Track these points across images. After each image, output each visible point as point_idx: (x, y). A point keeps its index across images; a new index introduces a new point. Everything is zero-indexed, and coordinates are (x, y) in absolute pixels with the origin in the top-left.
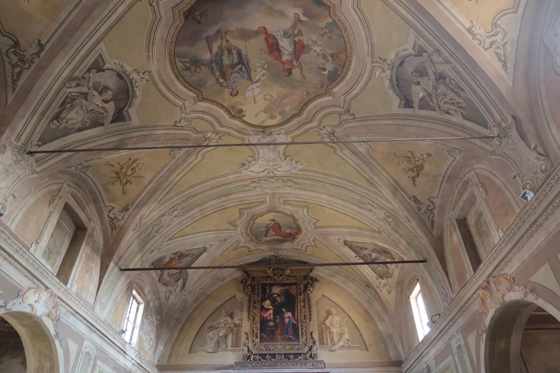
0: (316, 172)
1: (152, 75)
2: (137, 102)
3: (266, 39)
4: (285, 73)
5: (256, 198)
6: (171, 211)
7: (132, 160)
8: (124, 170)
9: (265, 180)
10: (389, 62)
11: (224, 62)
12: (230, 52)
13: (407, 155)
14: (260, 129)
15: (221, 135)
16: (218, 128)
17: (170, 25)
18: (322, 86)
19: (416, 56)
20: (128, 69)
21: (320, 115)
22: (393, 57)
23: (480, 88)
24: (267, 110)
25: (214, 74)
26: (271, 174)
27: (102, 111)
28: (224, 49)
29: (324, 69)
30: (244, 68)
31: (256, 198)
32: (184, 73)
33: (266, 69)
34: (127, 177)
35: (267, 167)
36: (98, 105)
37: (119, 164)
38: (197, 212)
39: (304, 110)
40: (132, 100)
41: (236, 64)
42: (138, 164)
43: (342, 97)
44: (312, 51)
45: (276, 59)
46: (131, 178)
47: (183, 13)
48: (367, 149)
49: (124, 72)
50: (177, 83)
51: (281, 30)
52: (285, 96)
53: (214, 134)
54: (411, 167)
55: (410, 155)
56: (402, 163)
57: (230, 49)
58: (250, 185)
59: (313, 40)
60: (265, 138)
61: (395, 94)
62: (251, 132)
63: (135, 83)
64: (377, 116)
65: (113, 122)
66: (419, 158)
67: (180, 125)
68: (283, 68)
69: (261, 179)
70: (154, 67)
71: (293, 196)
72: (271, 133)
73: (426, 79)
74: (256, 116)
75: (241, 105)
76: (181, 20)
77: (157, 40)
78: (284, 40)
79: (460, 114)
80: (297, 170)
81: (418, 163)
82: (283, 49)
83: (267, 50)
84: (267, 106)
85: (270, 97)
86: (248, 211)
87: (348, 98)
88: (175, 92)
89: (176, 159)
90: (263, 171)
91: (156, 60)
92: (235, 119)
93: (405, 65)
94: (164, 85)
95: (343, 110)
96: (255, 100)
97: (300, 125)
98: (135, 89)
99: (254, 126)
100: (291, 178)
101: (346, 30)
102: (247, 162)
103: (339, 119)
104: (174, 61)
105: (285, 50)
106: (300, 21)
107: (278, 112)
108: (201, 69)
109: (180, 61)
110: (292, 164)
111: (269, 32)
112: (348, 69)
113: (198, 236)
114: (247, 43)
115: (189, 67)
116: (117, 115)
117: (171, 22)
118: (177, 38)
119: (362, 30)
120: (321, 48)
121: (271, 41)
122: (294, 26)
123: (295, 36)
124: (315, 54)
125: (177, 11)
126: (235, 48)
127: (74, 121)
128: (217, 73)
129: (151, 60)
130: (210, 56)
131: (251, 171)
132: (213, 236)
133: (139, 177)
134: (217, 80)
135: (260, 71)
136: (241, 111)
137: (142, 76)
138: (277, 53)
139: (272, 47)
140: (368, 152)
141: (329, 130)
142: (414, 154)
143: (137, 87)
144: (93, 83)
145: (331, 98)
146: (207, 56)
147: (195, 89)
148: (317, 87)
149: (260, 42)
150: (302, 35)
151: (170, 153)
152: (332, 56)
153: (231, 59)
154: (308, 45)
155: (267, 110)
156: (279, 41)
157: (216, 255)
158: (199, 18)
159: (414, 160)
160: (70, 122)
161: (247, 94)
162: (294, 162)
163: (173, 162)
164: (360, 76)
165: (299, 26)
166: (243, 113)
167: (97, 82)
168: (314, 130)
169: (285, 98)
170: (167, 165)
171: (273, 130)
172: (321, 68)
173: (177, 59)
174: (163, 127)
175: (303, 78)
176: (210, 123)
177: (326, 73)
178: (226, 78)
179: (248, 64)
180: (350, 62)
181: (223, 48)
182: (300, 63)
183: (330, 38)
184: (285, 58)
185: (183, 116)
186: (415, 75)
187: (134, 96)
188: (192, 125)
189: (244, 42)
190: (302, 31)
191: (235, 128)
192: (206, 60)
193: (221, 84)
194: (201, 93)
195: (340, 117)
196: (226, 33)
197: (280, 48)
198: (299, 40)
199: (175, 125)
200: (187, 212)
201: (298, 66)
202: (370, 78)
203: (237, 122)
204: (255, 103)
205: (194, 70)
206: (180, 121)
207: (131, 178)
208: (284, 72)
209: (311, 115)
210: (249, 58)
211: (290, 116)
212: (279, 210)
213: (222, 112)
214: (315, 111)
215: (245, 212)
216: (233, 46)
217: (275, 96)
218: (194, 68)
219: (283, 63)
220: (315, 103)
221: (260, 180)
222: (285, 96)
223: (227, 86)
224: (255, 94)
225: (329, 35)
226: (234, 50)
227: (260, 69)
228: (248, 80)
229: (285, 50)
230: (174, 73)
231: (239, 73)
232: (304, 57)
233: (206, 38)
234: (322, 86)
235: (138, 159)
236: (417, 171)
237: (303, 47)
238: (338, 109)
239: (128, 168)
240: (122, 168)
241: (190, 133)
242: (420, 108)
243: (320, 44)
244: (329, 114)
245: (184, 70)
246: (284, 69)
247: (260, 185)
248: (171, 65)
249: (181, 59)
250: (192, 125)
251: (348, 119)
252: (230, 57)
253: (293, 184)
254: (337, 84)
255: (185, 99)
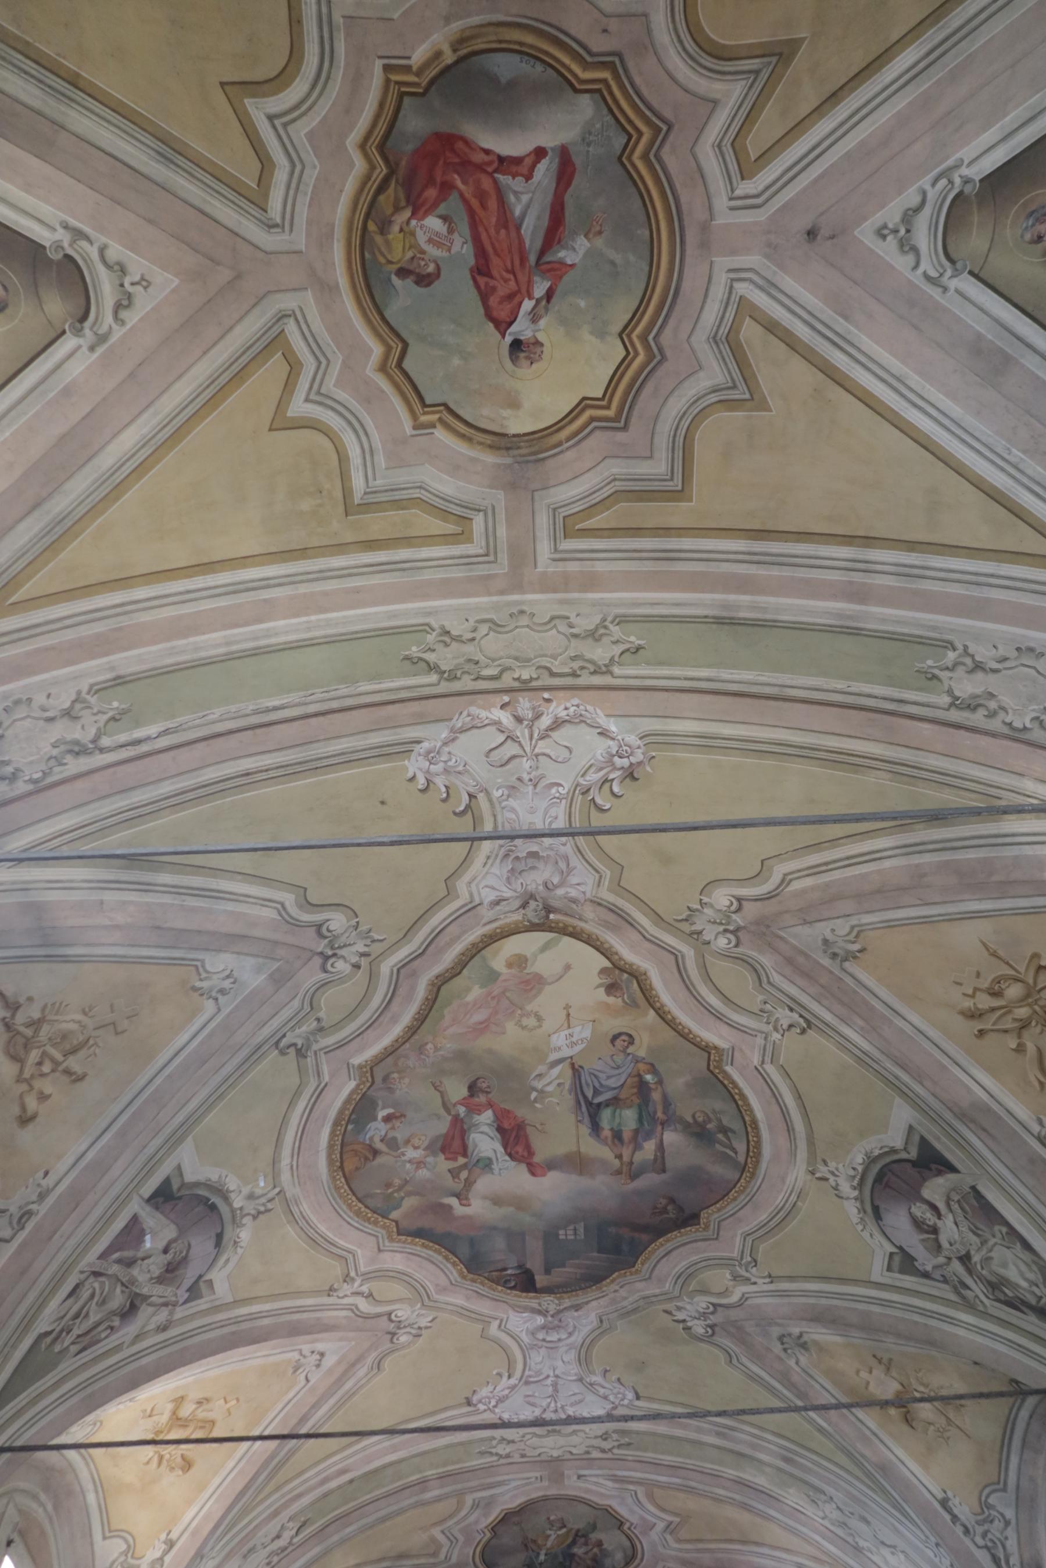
0: (348, 759)
1: (809, 1164)
2: (873, 1144)
3: (531, 1153)
4: (484, 1085)
5: (600, 567)
6: (977, 718)
7: (976, 1025)
8: (1022, 1012)
9: (553, 674)
10: (245, 1220)
11: (636, 1116)
12: (617, 1135)
13: (82, 1054)
14: (557, 922)
15: (686, 927)
16: (688, 952)
17: (731, 1219)
18: (385, 1079)
19: (200, 1276)
20: (852, 1209)
21: (377, 1000)
22: (241, 1235)
23: (56, 1400)
24: (534, 984)
25: (665, 1097)
26: (524, 705)
27: (955, 1207)
28: (630, 1142)
29: (387, 1119)
30: (589, 1094)
31: (600, 567)
32: (736, 1125)
33: (534, 1089)
34: (1031, 981)
35: (542, 747)
36: (956, 1224)
37: (1020, 1049)
38: (883, 602)
39: (427, 999)
40: (880, 1156)
41: (607, 1105)
42: (973, 996)
43: (327, 1078)
44: (423, 1146)
45: (509, 1112)
46: (1022, 970)
47: (699, 1224)
48: (204, 975)
49: (865, 1212)
50: (759, 1114)
51: (496, 1171)
52: (482, 1028)
53: (707, 936)
54: (45, 1030)
55: (74, 1063)
56: (79, 1017)
57: (616, 1141)
58: (618, 649)
59: (425, 1167)
60: (545, 884)
61: (203, 1181)
62: (589, 912)
63: (854, 1177)
64: (221, 1097)
65: (953, 1169)
66: (43, 1075)
67: (796, 1016)
68: (490, 1096)
69: (569, 681)
70: (798, 1174)
71: (427, 575)
72: (524, 906)
73: (156, 1275)
74: (568, 967)
75: (607, 1005)
76: (707, 1218)
77: (770, 1211)
78: (490, 1154)
79: (49, 1329)
80: (426, 745)
81: (34, 1055)
82: (492, 1135)
83: (529, 1130)
84: (535, 996)
85: (525, 1021)
86: (644, 468)
87: (313, 1084)
88: (774, 1100)
89: (854, 921)
90: (557, 724)
91: (788, 1183)
92: (631, 965)
93: (210, 1245)
94: (793, 1130)
95: (315, 1047)
96: (568, 1015)
97: (431, 948)
98: (860, 1169)
99: (576, 934)
100: (444, 687)
101: (358, 1213)
102: (616, 789)
103: (322, 1014)
104: (749, 1160)
105: (487, 1134)
106: (457, 1196)
107: (501, 978)
108: (693, 1116)
109: (736, 1153)
110: (446, 771)
111: (523, 1167)
112: (331, 1147)
113: (942, 418)
114: (575, 1149)
115: (720, 1132)
116: (933, 1166)
117: (728, 1221)
118: (727, 1194)
119: (325, 1231)
120: (403, 1158)
121: (520, 1149)
122: (469, 1183)
123: (464, 1166)
124: (416, 1142)
125: (710, 1232)
126: (604, 1142)
127: (1023, 1267)
128: (656, 1096)
129: (797, 1190)
130: (665, 1137)
131: (604, 734)
132: (867, 344)
133: (994, 954)
134: (660, 1082)
135: (548, 1084)
136: (611, 988)
137: (832, 1179)
138: (506, 1126)
139: (517, 1137)
140: (198, 968)
141: (341, 966)
142: (65, 1079)
143: (854, 1169)
144: (936, 1257)
145: (357, 1060)
146: (670, 1137)
147: (722, 1082)
148: (399, 1072)
149: (544, 1149)
150: (449, 1171)
151: (860, 951)
152: (376, 1153)
153: (617, 1120)
154: (434, 1154)
155: (534, 984)
156: (500, 1149)
157: (914, 74)
158: (670, 1208)
159: (53, 1060)
160: (1031, 1276)
161: (587, 1033)
162: (440, 782)
163: (867, 919)
164: (298, 1151)
165: (458, 1186)
166: (609, 981)
167: (926, 1248)
168: (385, 945)
169: (481, 1023)
170: (890, 925)
171: (517, 917)
172: (397, 1118)
173: (741, 1159)
174: (845, 1045)
175: (438, 1083)
176: (707, 978)
177: (381, 1114)
178: (636, 1079)
179: (578, 1102)
180: (330, 1162)
181: (631, 1147)
182: (449, 1113)
183: (388, 1185)
184: (488, 1116)
185: (776, 1036)
186: (181, 1252)
187: (871, 1161)
188: (761, 998)
189: (582, 1150)
190: (451, 1178)
191: (635, 936)
192: (675, 1130)
193: (653, 1070)
194: (709, 1065)
195: (318, 1020)
196: (619, 1172)
197: (498, 1136)
198: (455, 1159)
199: (809, 1027)
200: (920, 641)
201: (455, 1105)
202: (275, 1161)
203: (628, 955)
204: (567, 1007)
205: (710, 1121)
206: (791, 1026)
207: (1022, 970)
208: (489, 1087)
209: (402, 991)
210: (573, 1117)
211: (465, 971)
212: (490, 458)
213: (666, 998)
214: (395, 1007)
215: (658, 467)
216: (606, 1144)
217: (510, 1026)
218: (709, 1126)
219: (490, 1105)
220: (397, 1030)
221: (574, 675)
222: (482, 1028)
223: (637, 1062)
224: (567, 1032)
225: (390, 1190)
226: (606, 1138)
227: (550, 1089)
228: (581, 1067)
229: (487, 1134)
230: (758, 1135)
231: (601, 1085)
232: (442, 1126)
233: (664, 1171)
234: (385, 1079)
235: (962, 1013)
236: (18, 1033)
237: (443, 1150)
238: (330, 1040)
239: (1008, 1009)
240: (1024, 1025)
241: (776, 978)
242: (135, 1219)
243: (408, 1165)
244: (352, 1015)
245: (734, 1132)
246: (488, 1093)
247: (577, 647)
248: (758, 1155)
249: (733, 1155)
250: (761, 998)
251: (292, 1029)
252: (619, 1124)
253: (431, 657)
254: (348, 1101)
255: (756, 1073)
